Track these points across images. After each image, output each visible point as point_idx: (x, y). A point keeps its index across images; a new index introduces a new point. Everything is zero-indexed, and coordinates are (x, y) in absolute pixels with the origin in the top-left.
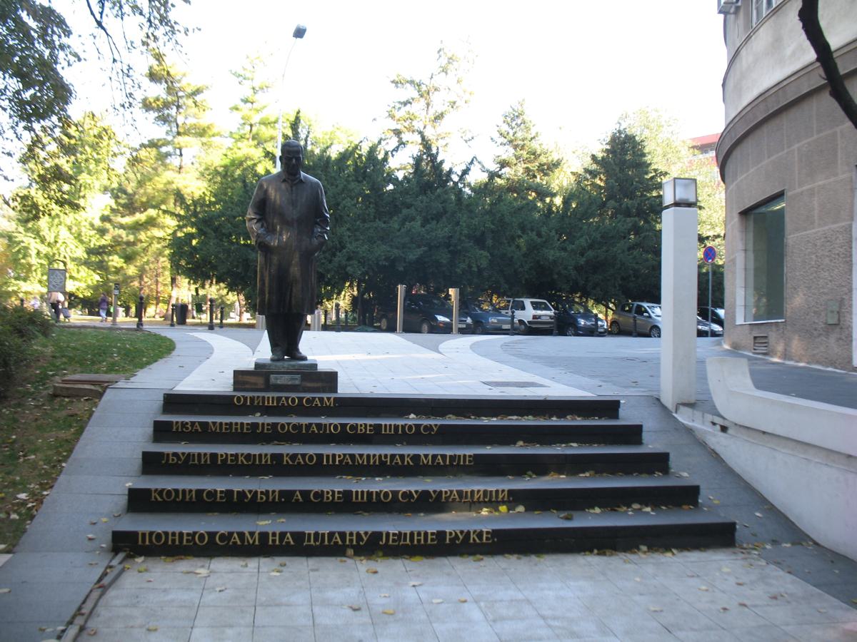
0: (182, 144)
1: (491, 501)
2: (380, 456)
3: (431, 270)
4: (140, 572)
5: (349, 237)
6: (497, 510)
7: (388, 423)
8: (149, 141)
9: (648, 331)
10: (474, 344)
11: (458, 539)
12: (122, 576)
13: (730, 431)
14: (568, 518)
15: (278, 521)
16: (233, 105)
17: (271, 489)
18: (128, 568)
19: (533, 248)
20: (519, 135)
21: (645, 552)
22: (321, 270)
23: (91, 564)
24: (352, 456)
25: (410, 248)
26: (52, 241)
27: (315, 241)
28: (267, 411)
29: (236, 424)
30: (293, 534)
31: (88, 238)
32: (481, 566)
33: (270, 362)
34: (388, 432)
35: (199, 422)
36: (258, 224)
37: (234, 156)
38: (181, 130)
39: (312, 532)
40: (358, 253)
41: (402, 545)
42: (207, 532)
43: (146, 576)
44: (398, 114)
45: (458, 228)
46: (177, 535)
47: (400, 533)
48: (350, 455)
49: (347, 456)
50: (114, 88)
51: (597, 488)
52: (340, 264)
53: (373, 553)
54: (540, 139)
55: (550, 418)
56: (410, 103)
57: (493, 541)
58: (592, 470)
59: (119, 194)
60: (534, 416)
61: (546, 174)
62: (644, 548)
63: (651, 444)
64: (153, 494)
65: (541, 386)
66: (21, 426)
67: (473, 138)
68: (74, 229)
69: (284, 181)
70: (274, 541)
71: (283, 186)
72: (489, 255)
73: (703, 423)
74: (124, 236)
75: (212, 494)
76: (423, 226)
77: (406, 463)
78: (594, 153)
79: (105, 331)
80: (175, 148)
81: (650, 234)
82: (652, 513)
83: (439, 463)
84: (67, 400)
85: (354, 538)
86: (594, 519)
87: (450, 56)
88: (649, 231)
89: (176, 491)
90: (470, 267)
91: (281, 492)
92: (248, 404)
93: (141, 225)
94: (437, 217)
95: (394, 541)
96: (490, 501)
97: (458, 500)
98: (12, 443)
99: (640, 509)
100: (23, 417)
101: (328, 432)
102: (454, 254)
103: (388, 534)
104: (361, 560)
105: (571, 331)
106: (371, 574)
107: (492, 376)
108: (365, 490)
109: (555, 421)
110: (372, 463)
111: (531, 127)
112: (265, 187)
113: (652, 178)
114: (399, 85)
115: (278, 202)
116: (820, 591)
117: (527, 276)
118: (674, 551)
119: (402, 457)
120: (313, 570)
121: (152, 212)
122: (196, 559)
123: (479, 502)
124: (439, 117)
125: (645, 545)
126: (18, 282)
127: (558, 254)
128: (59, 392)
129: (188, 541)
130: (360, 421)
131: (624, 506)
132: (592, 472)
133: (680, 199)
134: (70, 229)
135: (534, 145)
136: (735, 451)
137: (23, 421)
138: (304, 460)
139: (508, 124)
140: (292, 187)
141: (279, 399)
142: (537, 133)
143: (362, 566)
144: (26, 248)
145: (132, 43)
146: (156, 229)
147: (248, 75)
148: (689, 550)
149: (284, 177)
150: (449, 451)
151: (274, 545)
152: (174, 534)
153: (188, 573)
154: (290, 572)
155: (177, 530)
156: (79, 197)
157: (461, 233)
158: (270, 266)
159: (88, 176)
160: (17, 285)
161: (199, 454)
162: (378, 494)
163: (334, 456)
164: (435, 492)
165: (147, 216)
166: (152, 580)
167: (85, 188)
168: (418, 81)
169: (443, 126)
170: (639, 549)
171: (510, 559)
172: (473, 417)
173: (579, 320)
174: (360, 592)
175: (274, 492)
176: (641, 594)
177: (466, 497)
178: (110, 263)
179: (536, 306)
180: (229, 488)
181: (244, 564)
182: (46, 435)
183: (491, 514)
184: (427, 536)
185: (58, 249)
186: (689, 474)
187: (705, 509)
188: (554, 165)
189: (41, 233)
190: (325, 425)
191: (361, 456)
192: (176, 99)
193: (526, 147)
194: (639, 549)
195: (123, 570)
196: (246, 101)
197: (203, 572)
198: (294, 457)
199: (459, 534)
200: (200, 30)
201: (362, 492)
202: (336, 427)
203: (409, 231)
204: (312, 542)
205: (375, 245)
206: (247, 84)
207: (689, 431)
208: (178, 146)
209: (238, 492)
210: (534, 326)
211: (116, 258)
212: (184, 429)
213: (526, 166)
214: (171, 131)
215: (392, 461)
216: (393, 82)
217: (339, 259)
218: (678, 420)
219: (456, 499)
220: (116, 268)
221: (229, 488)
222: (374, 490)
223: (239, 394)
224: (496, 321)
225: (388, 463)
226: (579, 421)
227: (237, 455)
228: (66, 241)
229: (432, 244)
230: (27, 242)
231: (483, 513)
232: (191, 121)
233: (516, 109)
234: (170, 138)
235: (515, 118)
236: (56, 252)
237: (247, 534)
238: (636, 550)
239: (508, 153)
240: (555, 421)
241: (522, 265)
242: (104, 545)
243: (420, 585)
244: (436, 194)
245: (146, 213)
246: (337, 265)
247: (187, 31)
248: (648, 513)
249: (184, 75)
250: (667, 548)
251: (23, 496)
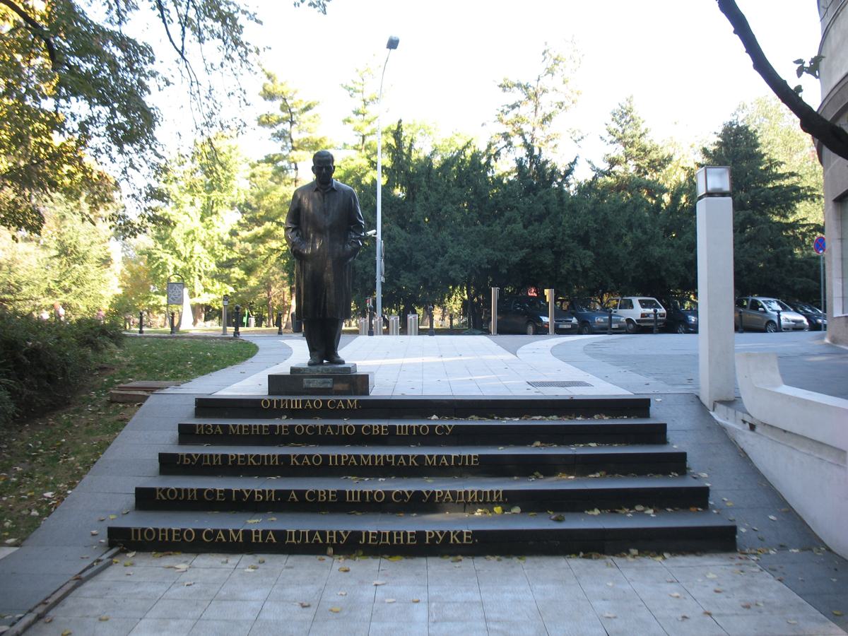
0: (296, 158)
1: (485, 501)
2: (385, 457)
3: (536, 272)
4: (125, 566)
5: (452, 242)
6: (492, 511)
7: (402, 425)
8: (265, 157)
9: (763, 327)
10: (554, 347)
13: (758, 429)
14: (558, 520)
15: (269, 519)
16: (346, 118)
17: (267, 489)
18: (116, 562)
19: (639, 245)
20: (628, 132)
21: (634, 556)
22: (424, 276)
23: (82, 558)
24: (357, 457)
25: (512, 250)
26: (188, 255)
27: (349, 248)
28: (293, 413)
29: (255, 426)
30: (275, 532)
31: (221, 252)
32: (456, 567)
33: (306, 366)
34: (402, 433)
35: (220, 425)
36: (293, 233)
37: (348, 167)
38: (295, 145)
40: (460, 257)
41: (382, 544)
42: (194, 530)
43: (129, 570)
44: (506, 118)
45: (560, 229)
46: (260, 533)
47: (379, 532)
50: (194, 110)
51: (605, 487)
52: (442, 269)
53: (354, 553)
54: (649, 136)
55: (575, 417)
56: (519, 106)
57: (474, 542)
58: (603, 470)
59: (245, 209)
60: (559, 417)
61: (657, 171)
62: (634, 552)
63: (676, 444)
64: (158, 494)
65: (587, 385)
66: (74, 430)
67: (582, 138)
68: (208, 244)
69: (317, 190)
70: (257, 539)
71: (316, 195)
72: (593, 254)
73: (735, 422)
74: (250, 248)
75: (212, 493)
76: (525, 227)
78: (705, 146)
79: (201, 341)
80: (290, 163)
81: (765, 226)
82: (653, 515)
83: (443, 464)
84: (121, 405)
85: (260, 536)
86: (592, 521)
87: (556, 57)
88: (764, 223)
89: (179, 490)
90: (575, 267)
91: (276, 491)
92: (275, 407)
93: (260, 238)
94: (540, 219)
95: (373, 540)
96: (485, 502)
97: (451, 500)
98: (59, 446)
99: (642, 511)
100: (77, 422)
101: (343, 433)
102: (559, 254)
103: (367, 533)
104: (340, 559)
105: (682, 328)
106: (342, 572)
107: (545, 376)
108: (359, 490)
109: (580, 421)
110: (376, 464)
111: (640, 124)
112: (299, 196)
113: (767, 169)
114: (507, 89)
115: (311, 210)
116: (804, 601)
117: (633, 275)
118: (666, 555)
119: (406, 457)
120: (287, 568)
121: (268, 225)
122: (183, 555)
123: (475, 503)
124: (547, 118)
125: (635, 548)
126: (158, 296)
127: (664, 251)
128: (115, 398)
129: (176, 537)
130: (375, 423)
131: (627, 508)
132: (603, 473)
133: (714, 189)
134: (204, 244)
135: (645, 142)
136: (761, 450)
137: (77, 426)
138: (310, 461)
139: (616, 121)
140: (323, 195)
141: (304, 402)
142: (646, 130)
143: (338, 563)
144: (164, 264)
145: (212, 65)
146: (274, 241)
147: (359, 88)
148: (683, 555)
149: (316, 186)
150: (454, 452)
151: (257, 543)
152: (163, 531)
153: (169, 567)
154: (265, 569)
155: (167, 527)
156: (212, 214)
157: (564, 234)
158: (305, 273)
159: (219, 193)
160: (157, 299)
161: (211, 456)
162: (371, 494)
163: (339, 456)
164: (428, 492)
165: (265, 229)
166: (131, 573)
167: (217, 203)
168: (525, 84)
169: (551, 128)
170: (628, 553)
171: (490, 560)
172: (496, 418)
173: (689, 317)
174: (320, 590)
175: (270, 491)
176: (604, 600)
177: (460, 498)
178: (232, 275)
179: (644, 304)
180: (227, 487)
181: (224, 559)
182: (91, 438)
183: (484, 515)
184: (172, 534)
185: (193, 264)
186: (708, 474)
187: (715, 511)
188: (665, 160)
189: (177, 249)
190: (341, 427)
191: (366, 456)
192: (290, 115)
193: (635, 144)
194: (628, 553)
195: (110, 564)
196: (357, 113)
197: (183, 566)
198: (301, 458)
199: (439, 534)
200: (270, 48)
201: (356, 492)
202: (350, 428)
203: (511, 233)
205: (477, 249)
206: (358, 96)
207: (722, 429)
208: (292, 160)
210: (642, 324)
211: (236, 270)
212: (207, 432)
213: (635, 163)
214: (286, 146)
216: (500, 86)
217: (442, 264)
218: (714, 419)
219: (450, 499)
220: (237, 279)
221: (228, 487)
222: (367, 490)
223: (275, 398)
224: (602, 321)
225: (393, 464)
226: (607, 421)
227: (246, 456)
228: (200, 256)
229: (535, 245)
230: (165, 258)
231: (476, 514)
232: (304, 135)
233: (624, 106)
234: (285, 153)
235: (624, 115)
236: (191, 266)
237: (231, 532)
238: (625, 554)
239: (618, 151)
240: (580, 421)
241: (627, 263)
242: (103, 541)
243: (383, 584)
244: (538, 195)
245: (263, 227)
246: (439, 270)
247: (258, 52)
248: (649, 515)
249: (295, 92)
250: (659, 552)
251: (49, 494)
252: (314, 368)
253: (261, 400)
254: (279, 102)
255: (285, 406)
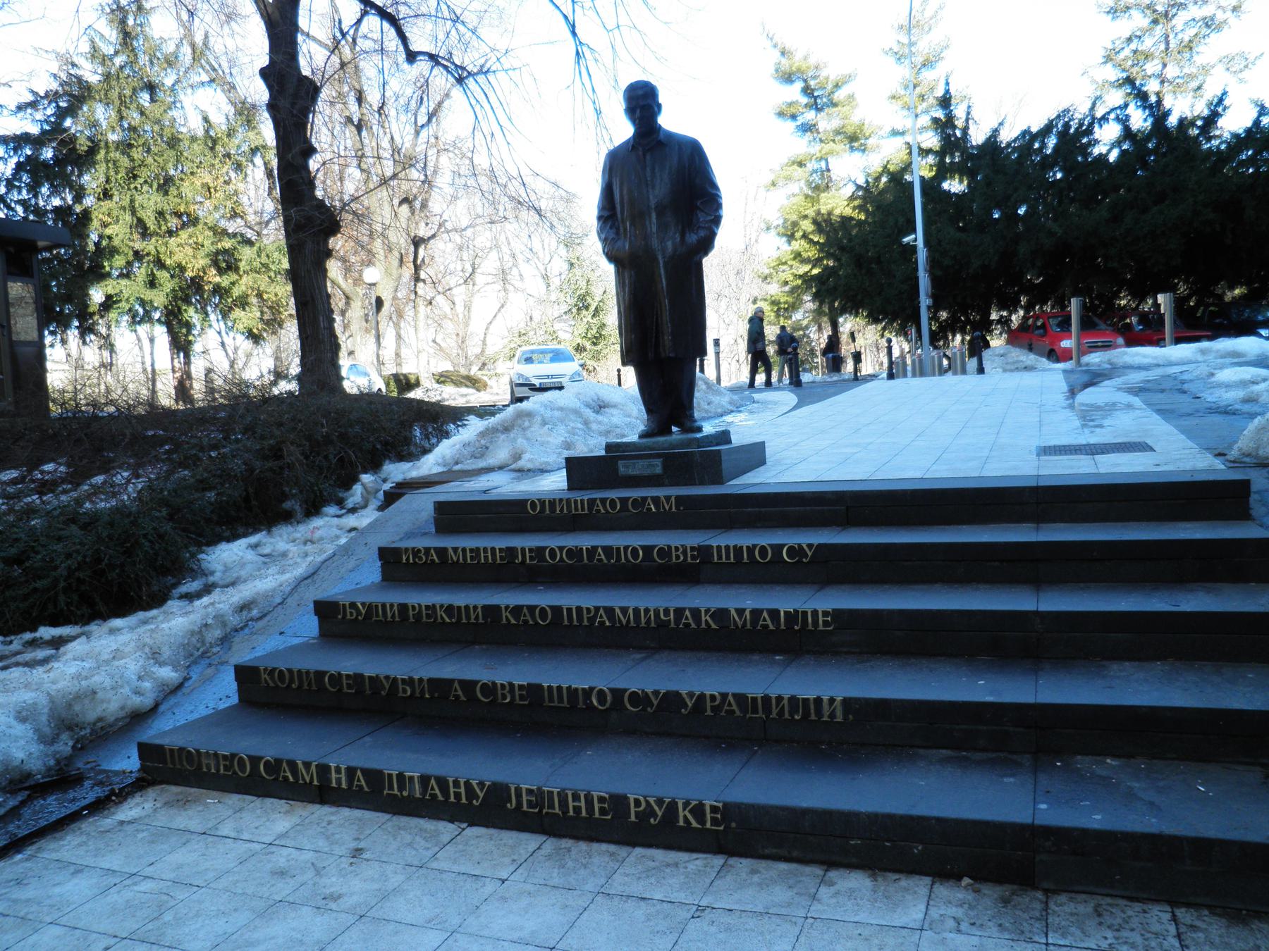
11: (654, 814)
12: (42, 843)
29: (485, 550)
39: (395, 773)
48: (605, 608)
49: (601, 611)
77: (704, 626)
141: (592, 502)
163: (579, 609)
198: (517, 610)
204: (396, 792)
209: (370, 678)
215: (678, 620)
223: (586, 496)
225: (673, 625)
252: (644, 440)
253: (526, 501)
254: (799, 85)
255: (562, 510)
